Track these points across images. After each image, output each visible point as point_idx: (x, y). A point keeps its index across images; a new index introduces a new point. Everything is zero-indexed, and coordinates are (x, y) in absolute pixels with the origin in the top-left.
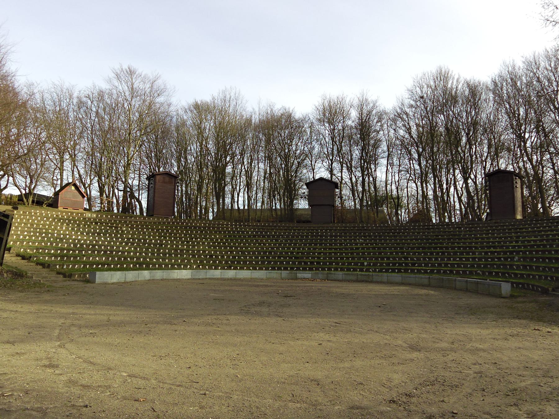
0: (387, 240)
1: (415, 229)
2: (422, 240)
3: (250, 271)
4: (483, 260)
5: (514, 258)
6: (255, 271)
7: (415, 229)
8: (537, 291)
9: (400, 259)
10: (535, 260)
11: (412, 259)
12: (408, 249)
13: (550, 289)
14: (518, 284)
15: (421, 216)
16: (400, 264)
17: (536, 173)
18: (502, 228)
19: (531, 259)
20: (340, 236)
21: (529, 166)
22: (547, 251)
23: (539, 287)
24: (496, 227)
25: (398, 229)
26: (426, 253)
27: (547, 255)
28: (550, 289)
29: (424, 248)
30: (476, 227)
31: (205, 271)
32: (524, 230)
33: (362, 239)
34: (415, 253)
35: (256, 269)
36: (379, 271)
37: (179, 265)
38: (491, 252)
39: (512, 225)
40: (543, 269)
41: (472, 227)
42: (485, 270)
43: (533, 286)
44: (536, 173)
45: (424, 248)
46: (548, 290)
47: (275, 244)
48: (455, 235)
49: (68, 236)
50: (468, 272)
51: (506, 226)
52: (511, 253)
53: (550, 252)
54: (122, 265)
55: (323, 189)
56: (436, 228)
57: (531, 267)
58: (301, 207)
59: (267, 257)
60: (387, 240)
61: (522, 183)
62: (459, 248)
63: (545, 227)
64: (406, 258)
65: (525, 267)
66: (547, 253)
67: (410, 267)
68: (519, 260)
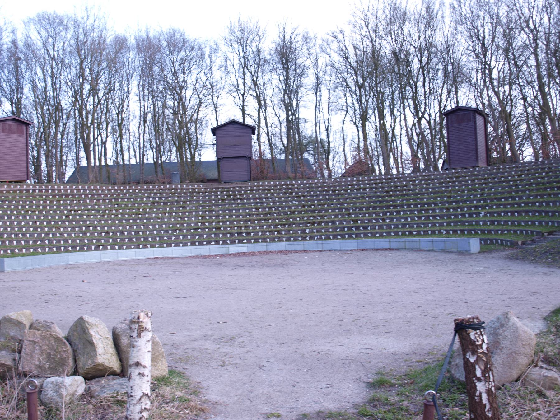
0: (314, 201)
1: (360, 185)
2: (370, 197)
3: (338, 241)
4: (445, 218)
5: (480, 213)
6: (344, 241)
7: (360, 185)
8: (507, 245)
9: (348, 222)
10: (502, 214)
11: (362, 221)
12: (355, 210)
13: (520, 243)
14: (486, 240)
15: (360, 168)
16: (350, 229)
17: (504, 110)
18: (464, 179)
19: (499, 214)
20: (267, 198)
21: (495, 100)
22: (516, 204)
23: (508, 241)
24: (457, 177)
25: (339, 186)
26: (377, 214)
27: (516, 208)
28: (520, 243)
29: (374, 208)
30: (494, 178)
31: (265, 244)
32: (489, 180)
33: (296, 201)
34: (365, 214)
35: (329, 239)
36: (326, 239)
37: (74, 247)
38: (453, 208)
39: (475, 175)
40: (511, 224)
41: (429, 180)
42: (449, 228)
43: (502, 240)
44: (504, 110)
45: (374, 208)
46: (517, 244)
47: (184, 213)
48: (409, 190)
49: (55, 207)
50: (407, 233)
51: (468, 176)
52: (476, 207)
53: (519, 205)
54: (35, 250)
55: (233, 134)
56: (386, 183)
57: (499, 222)
58: (204, 159)
59: (23, 235)
60: (314, 201)
61: (486, 122)
62: (416, 205)
63: (514, 176)
64: (356, 221)
65: (492, 223)
66: (516, 206)
67: (400, 229)
68: (485, 215)
